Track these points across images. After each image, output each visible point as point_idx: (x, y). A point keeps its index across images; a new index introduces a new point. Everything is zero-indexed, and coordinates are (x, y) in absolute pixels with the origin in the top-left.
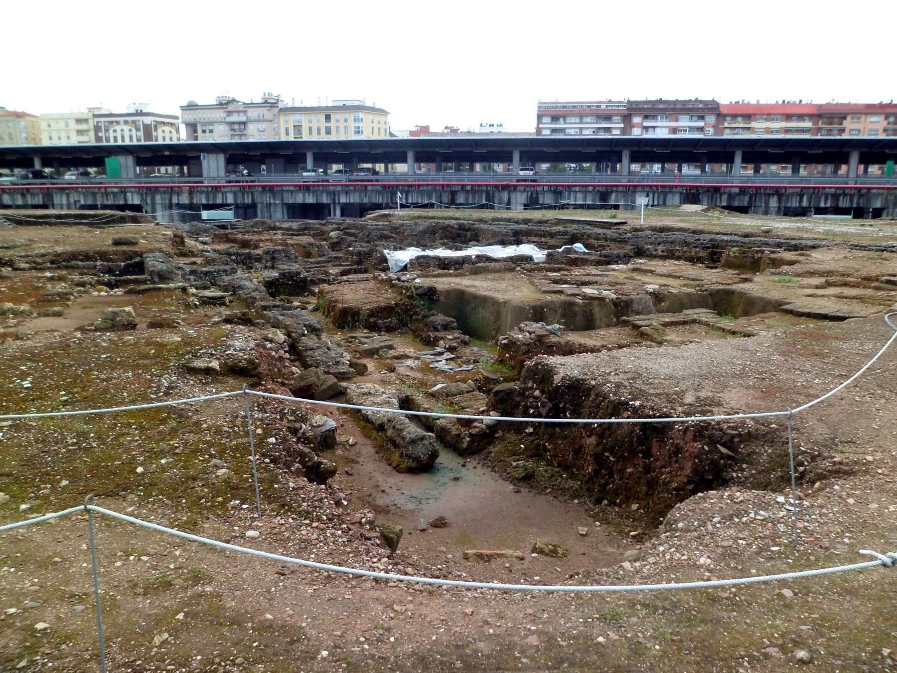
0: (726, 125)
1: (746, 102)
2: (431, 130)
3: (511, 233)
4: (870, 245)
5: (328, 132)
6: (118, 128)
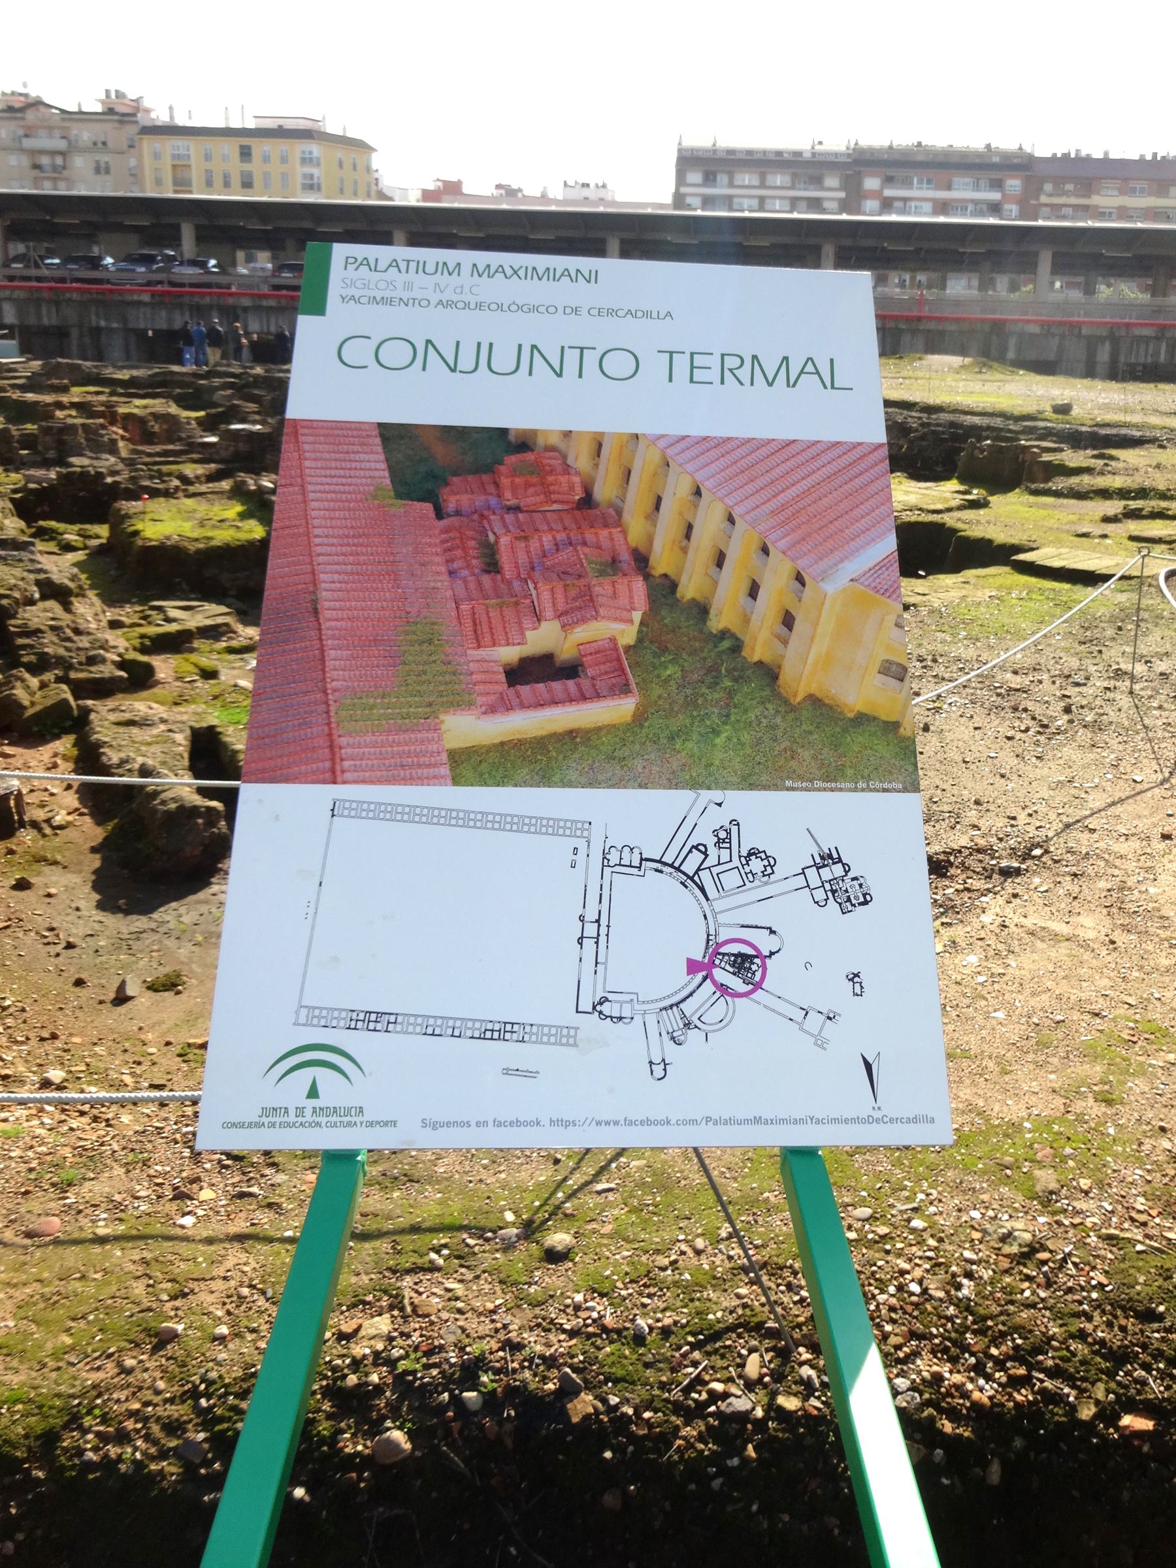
0: (1044, 199)
1: (1083, 154)
2: (466, 190)
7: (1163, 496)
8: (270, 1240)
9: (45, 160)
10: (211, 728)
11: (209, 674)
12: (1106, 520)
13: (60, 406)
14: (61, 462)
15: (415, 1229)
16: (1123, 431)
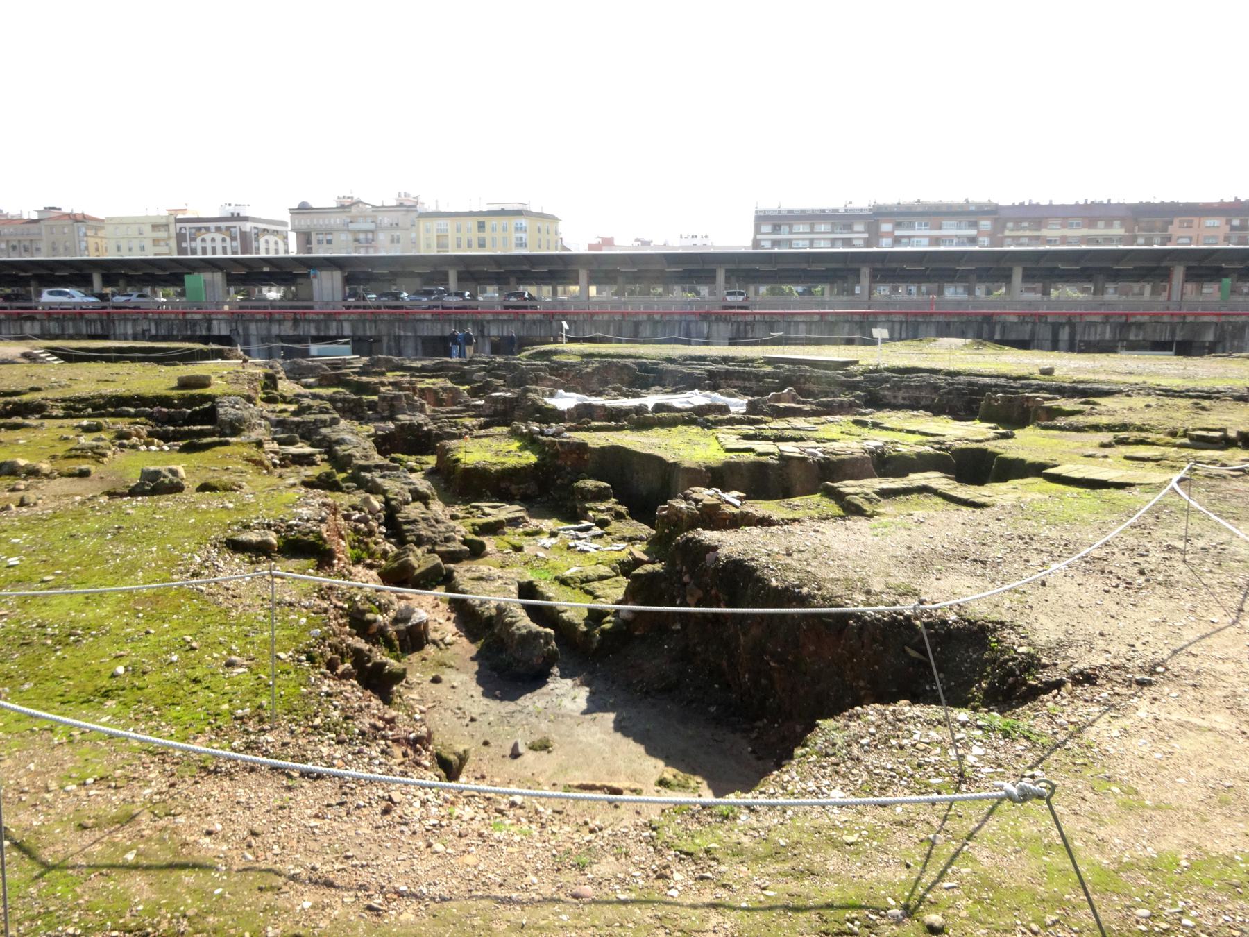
0: (1007, 233)
1: (1034, 202)
2: (616, 243)
3: (705, 375)
4: (1188, 390)
5: (482, 245)
6: (208, 237)
7: (1140, 429)
8: (734, 909)
9: (362, 236)
10: (530, 583)
11: (518, 549)
12: (1103, 445)
13: (382, 384)
14: (392, 418)
15: (829, 906)
16: (1096, 386)
